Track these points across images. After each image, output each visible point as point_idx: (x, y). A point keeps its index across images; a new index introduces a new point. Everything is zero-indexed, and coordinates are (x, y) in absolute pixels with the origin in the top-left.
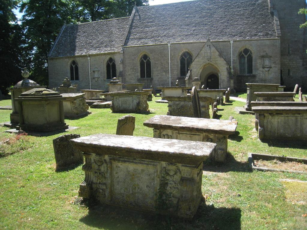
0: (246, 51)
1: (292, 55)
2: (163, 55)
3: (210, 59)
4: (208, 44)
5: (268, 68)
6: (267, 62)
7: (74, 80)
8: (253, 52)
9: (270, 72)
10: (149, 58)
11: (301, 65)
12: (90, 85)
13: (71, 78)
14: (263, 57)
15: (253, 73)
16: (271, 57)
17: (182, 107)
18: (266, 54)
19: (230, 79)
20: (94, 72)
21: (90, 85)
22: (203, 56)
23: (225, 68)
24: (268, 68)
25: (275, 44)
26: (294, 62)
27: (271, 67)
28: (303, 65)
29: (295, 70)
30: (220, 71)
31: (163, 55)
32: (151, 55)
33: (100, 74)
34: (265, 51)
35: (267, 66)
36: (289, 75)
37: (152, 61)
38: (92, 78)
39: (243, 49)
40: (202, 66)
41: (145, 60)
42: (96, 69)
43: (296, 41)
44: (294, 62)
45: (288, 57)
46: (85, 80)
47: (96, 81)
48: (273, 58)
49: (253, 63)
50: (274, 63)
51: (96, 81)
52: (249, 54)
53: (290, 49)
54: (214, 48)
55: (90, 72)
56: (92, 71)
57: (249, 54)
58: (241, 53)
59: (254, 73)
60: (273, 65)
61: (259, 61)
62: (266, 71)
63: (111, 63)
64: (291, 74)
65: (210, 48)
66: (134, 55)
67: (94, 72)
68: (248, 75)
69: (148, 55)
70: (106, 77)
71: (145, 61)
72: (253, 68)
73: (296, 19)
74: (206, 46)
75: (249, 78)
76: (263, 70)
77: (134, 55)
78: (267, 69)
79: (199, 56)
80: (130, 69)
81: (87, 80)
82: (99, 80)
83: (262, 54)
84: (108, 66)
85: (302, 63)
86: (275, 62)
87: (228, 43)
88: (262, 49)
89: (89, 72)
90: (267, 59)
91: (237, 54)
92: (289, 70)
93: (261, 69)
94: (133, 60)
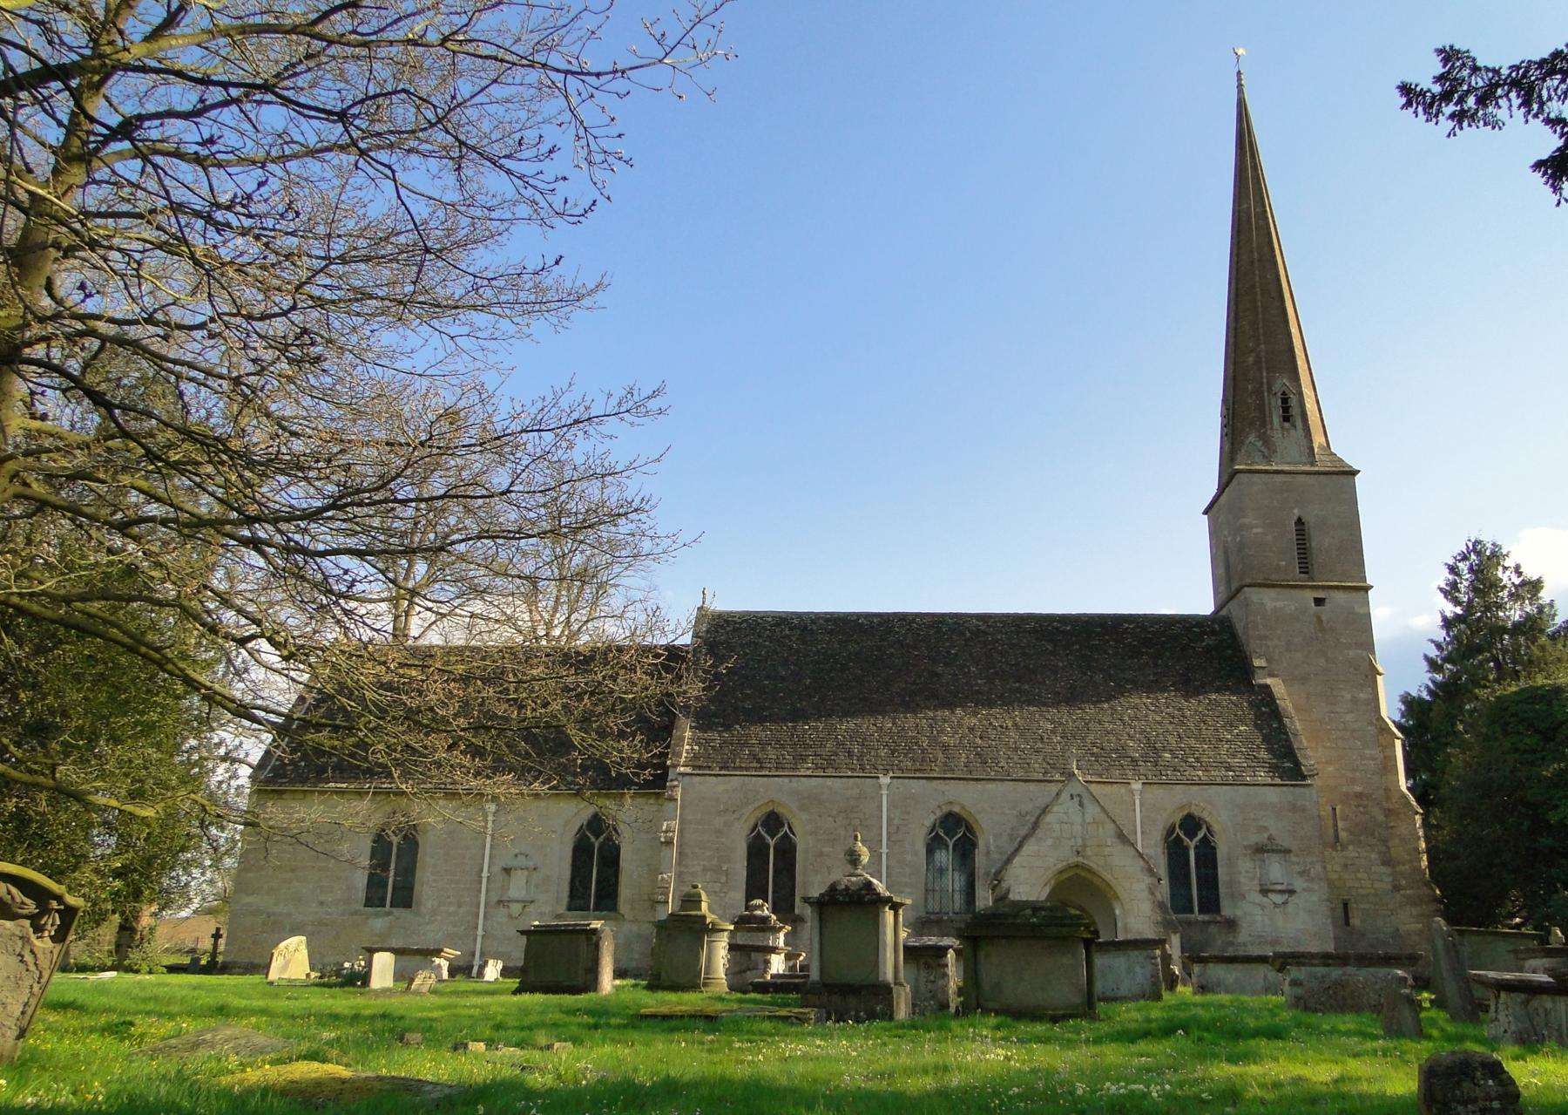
0: (1191, 823)
1: (1351, 847)
2: (857, 822)
3: (1084, 846)
4: (1075, 792)
5: (1281, 892)
6: (1276, 870)
7: (384, 906)
8: (1216, 827)
9: (1290, 908)
10: (790, 828)
11: (1389, 887)
12: (480, 932)
13: (572, 896)
14: (1260, 850)
15: (1223, 913)
16: (1288, 851)
17: (1339, 984)
18: (1270, 838)
19: (1164, 927)
20: (507, 871)
21: (480, 932)
22: (1054, 835)
23: (1143, 886)
24: (1281, 892)
25: (1299, 803)
26: (1359, 875)
27: (1291, 892)
28: (1396, 888)
29: (1367, 906)
30: (1121, 893)
31: (857, 822)
32: (805, 816)
33: (537, 886)
34: (1266, 829)
35: (1279, 887)
36: (1347, 923)
37: (802, 843)
38: (495, 899)
39: (1177, 818)
40: (1050, 873)
41: (597, 837)
42: (521, 861)
43: (1360, 796)
44: (1359, 875)
45: (1334, 854)
46: (452, 909)
47: (510, 916)
48: (1297, 855)
49: (1221, 871)
50: (1303, 873)
51: (510, 916)
52: (1201, 835)
53: (1340, 824)
54: (1098, 809)
55: (485, 874)
56: (497, 869)
57: (1201, 835)
58: (1171, 830)
59: (1227, 910)
60: (1299, 884)
61: (1245, 865)
62: (1276, 905)
63: (597, 837)
64: (1355, 921)
65: (1081, 805)
66: (726, 811)
67: (507, 871)
68: (1206, 917)
69: (789, 816)
70: (361, 894)
71: (772, 843)
72: (1222, 890)
73: (1349, 717)
74: (1065, 796)
75: (1213, 929)
76: (1265, 899)
77: (726, 811)
78: (1278, 899)
79: (1039, 832)
80: (699, 868)
81: (461, 911)
82: (527, 910)
83: (1255, 838)
84: (581, 851)
85: (1390, 879)
86: (1304, 872)
87: (1123, 790)
88: (1255, 820)
89: (482, 871)
90: (1274, 857)
91: (1158, 835)
92: (1346, 905)
93: (1259, 898)
94: (719, 832)
